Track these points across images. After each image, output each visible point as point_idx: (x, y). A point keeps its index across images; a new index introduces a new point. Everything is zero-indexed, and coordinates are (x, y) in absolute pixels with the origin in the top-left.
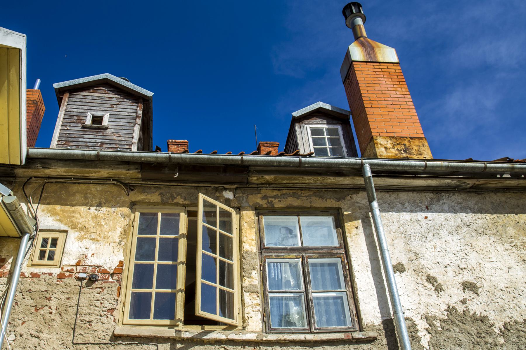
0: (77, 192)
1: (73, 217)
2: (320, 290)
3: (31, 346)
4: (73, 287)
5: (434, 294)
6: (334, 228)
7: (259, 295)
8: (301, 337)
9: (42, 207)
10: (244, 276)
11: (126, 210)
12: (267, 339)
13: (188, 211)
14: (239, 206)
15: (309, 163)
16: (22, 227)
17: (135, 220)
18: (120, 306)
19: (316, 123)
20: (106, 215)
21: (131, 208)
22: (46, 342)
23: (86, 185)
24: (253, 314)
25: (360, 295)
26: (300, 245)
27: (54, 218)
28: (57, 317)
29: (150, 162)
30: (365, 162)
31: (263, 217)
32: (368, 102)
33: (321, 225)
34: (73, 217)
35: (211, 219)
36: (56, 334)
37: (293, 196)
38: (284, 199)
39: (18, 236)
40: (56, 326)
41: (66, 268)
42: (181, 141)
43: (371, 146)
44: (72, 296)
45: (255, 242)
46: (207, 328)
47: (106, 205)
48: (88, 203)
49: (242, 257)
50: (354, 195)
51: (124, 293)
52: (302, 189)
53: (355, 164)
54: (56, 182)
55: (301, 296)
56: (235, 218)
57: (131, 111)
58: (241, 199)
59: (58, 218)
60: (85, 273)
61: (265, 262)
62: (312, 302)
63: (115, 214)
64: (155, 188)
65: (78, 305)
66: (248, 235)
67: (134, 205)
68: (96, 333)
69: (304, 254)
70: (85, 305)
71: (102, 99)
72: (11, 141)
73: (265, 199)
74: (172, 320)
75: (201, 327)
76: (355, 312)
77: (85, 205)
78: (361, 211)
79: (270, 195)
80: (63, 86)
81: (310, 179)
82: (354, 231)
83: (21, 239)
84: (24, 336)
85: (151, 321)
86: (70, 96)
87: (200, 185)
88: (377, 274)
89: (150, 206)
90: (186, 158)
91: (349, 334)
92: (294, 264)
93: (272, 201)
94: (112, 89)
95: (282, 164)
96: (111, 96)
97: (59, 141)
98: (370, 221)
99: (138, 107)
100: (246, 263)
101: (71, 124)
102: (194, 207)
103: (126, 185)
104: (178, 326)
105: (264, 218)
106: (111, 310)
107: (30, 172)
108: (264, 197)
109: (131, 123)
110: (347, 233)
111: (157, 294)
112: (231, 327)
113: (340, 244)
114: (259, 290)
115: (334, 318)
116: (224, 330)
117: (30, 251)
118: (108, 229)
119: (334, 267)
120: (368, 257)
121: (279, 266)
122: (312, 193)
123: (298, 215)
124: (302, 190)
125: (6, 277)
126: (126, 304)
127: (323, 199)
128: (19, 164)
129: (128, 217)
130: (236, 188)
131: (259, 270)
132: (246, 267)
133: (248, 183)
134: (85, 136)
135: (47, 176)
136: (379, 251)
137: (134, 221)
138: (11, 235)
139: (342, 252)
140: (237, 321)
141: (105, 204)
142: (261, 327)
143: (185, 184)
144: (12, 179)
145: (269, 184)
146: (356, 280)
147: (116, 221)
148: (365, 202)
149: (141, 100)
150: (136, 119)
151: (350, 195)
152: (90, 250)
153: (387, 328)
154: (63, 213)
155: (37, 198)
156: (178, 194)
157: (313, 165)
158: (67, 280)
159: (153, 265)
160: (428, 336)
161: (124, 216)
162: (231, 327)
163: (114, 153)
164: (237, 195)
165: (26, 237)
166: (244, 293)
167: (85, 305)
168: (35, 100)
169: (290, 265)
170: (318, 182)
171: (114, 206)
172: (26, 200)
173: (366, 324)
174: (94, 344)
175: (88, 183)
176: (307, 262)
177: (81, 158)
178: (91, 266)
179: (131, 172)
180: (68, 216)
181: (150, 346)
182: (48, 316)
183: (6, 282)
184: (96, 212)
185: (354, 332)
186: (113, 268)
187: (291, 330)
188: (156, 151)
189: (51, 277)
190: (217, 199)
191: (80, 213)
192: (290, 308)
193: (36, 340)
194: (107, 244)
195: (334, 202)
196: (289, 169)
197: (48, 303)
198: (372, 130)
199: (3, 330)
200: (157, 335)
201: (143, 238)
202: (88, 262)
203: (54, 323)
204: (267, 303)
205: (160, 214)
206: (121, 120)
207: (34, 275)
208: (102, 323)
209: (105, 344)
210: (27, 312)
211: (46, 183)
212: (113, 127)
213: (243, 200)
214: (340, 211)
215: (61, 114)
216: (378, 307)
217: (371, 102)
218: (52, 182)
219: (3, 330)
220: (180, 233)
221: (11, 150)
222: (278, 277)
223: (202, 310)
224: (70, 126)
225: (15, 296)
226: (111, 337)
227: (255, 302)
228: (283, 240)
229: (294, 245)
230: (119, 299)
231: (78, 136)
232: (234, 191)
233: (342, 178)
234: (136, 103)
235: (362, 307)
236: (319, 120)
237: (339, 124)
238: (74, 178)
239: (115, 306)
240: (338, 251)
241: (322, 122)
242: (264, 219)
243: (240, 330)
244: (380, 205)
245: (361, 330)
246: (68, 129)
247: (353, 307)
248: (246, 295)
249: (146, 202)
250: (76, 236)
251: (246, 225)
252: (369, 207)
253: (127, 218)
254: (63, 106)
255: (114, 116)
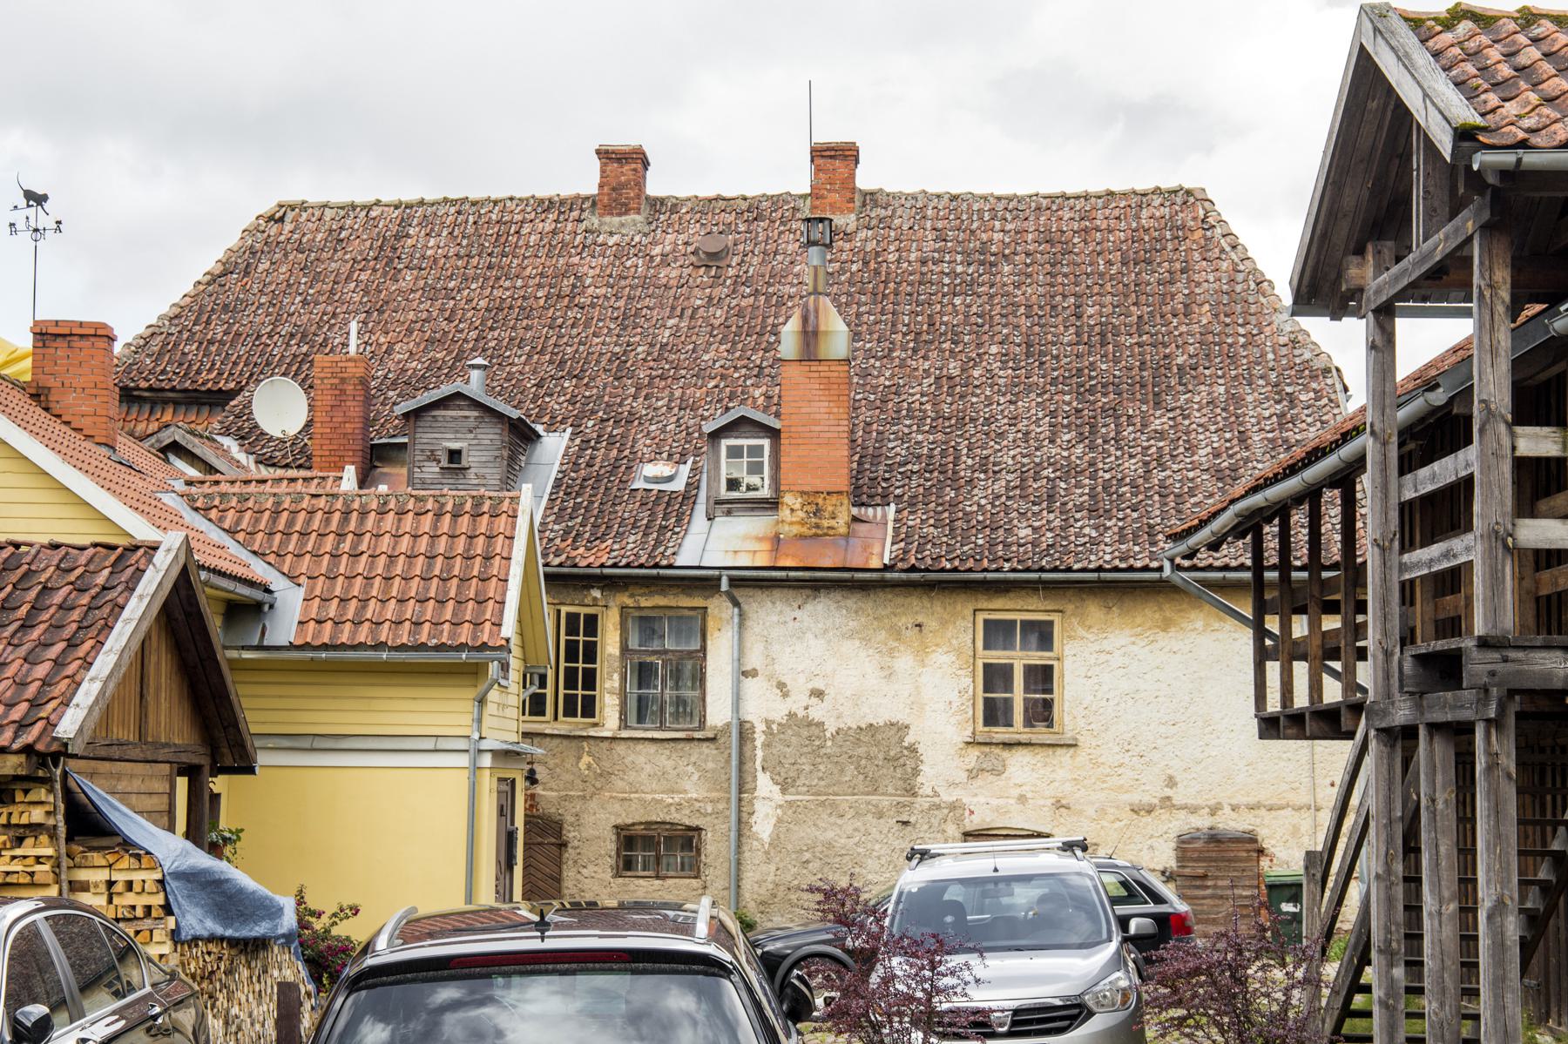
5: (779, 698)
160: (1172, 885)
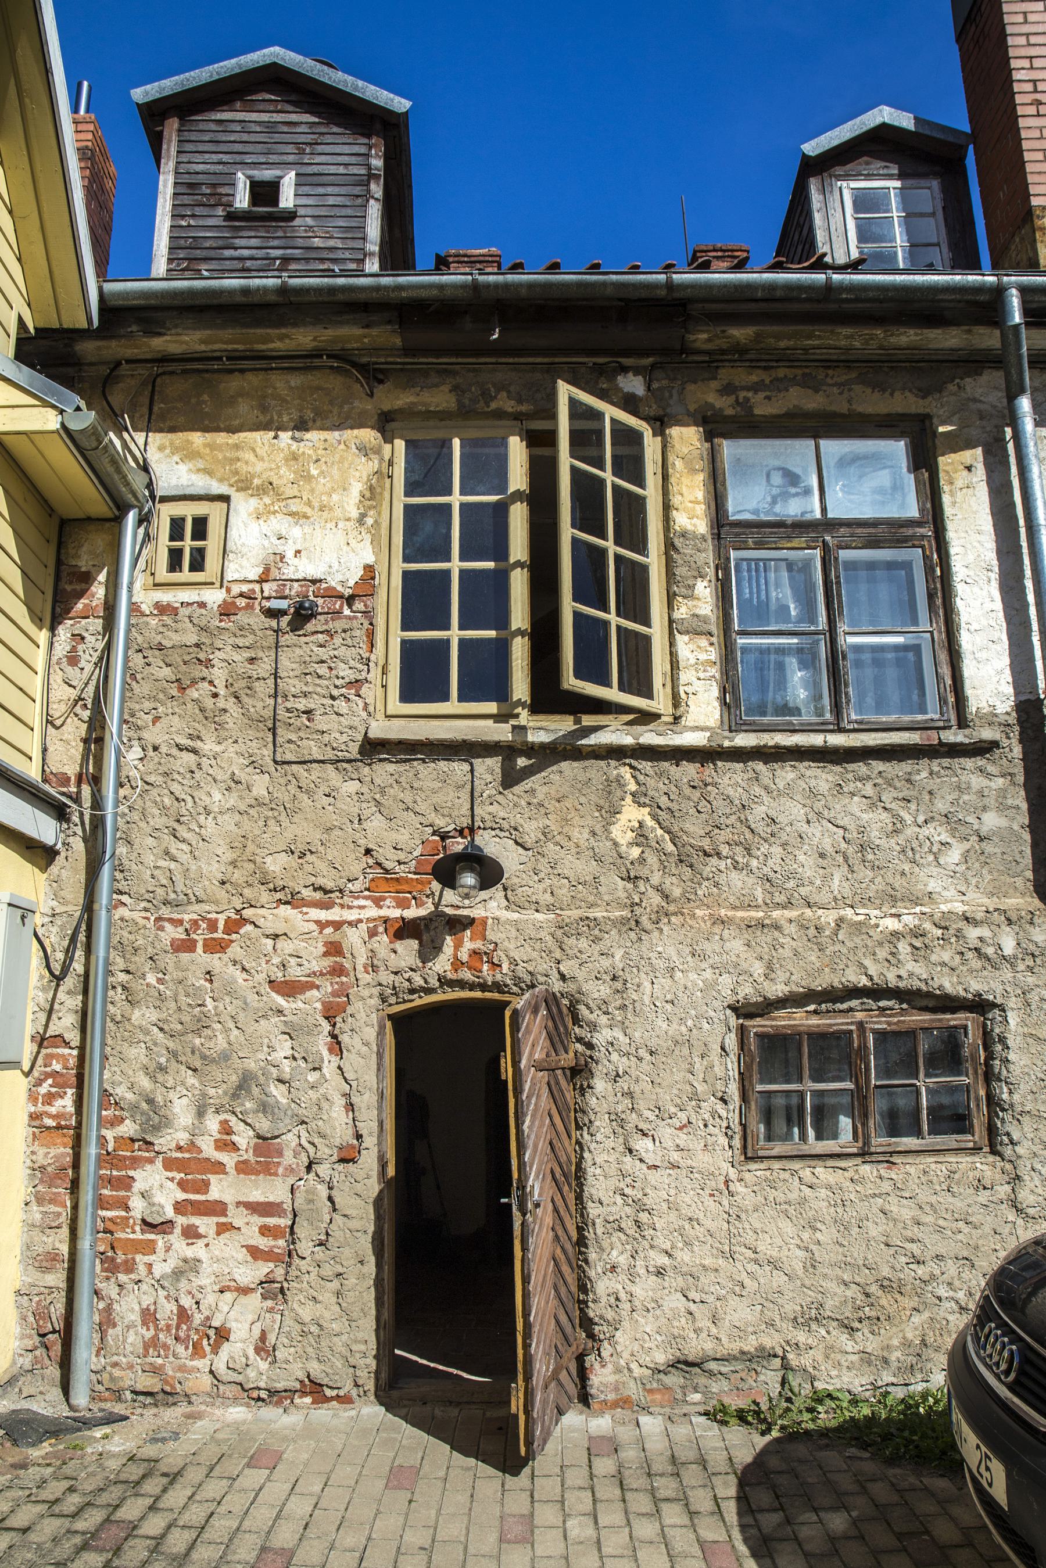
0: (241, 395)
1: (238, 460)
2: (864, 629)
3: (182, 770)
4: (259, 633)
6: (909, 471)
7: (714, 640)
8: (817, 740)
9: (156, 439)
10: (675, 594)
11: (369, 435)
12: (732, 744)
13: (527, 431)
14: (661, 413)
15: (852, 288)
16: (119, 491)
17: (395, 460)
18: (375, 674)
19: (868, 175)
20: (320, 452)
21: (382, 430)
22: (213, 762)
23: (261, 375)
24: (698, 686)
25: (966, 640)
26: (818, 515)
27: (191, 465)
28: (231, 704)
29: (423, 300)
30: (1009, 283)
31: (725, 443)
32: (1028, 98)
33: (874, 460)
34: (238, 460)
35: (592, 452)
36: (236, 742)
37: (804, 385)
38: (780, 391)
39: (110, 515)
40: (231, 725)
41: (236, 589)
42: (481, 251)
43: (1022, 239)
44: (260, 654)
45: (703, 507)
46: (588, 720)
47: (318, 423)
48: (271, 421)
49: (670, 546)
50: (968, 380)
51: (384, 642)
52: (828, 364)
53: (980, 289)
54: (185, 372)
55: (818, 641)
56: (651, 445)
57: (353, 160)
58: (667, 394)
59: (201, 464)
60: (285, 598)
61: (728, 559)
62: (844, 658)
63: (342, 446)
64: (438, 372)
65: (276, 676)
66: (684, 490)
67: (388, 421)
68: (326, 738)
69: (828, 538)
70: (291, 674)
71: (271, 127)
72: (54, 263)
73: (728, 395)
74: (503, 704)
75: (572, 718)
76: (949, 682)
77: (265, 427)
78: (984, 423)
79: (743, 383)
80: (158, 96)
81: (851, 337)
82: (962, 478)
83: (120, 523)
84: (164, 749)
85: (453, 707)
86: (181, 125)
87: (557, 360)
88: (1012, 589)
89: (431, 423)
90: (519, 285)
91: (933, 734)
92: (800, 565)
93: (747, 400)
94: (293, 98)
95: (779, 294)
96: (294, 117)
97: (170, 260)
98: (1006, 450)
99: (370, 149)
100: (680, 562)
101: (197, 209)
102: (543, 419)
103: (363, 368)
104: (517, 716)
105: (728, 446)
106: (356, 684)
107: (116, 349)
108: (728, 389)
109: (357, 196)
110: (942, 482)
111: (462, 642)
112: (646, 717)
113: (921, 510)
114: (714, 629)
115: (894, 696)
116: (629, 723)
117: (145, 552)
118: (329, 485)
119: (903, 572)
120: (992, 545)
121: (762, 569)
122: (854, 375)
123: (816, 436)
124: (829, 367)
125: (98, 617)
126: (390, 668)
127: (884, 390)
128: (86, 326)
129: (375, 453)
130: (653, 366)
131: (713, 579)
132: (680, 571)
133: (685, 349)
134: (238, 242)
135: (159, 356)
136: (1023, 531)
137: (391, 463)
138: (93, 515)
139: (928, 531)
140: (660, 703)
141: (314, 421)
142: (717, 715)
143: (516, 360)
144: (70, 371)
145: (739, 353)
146: (959, 604)
147: (346, 465)
148: (997, 398)
149: (378, 126)
150: (368, 185)
151: (957, 381)
152: (290, 542)
153: (1026, 721)
154: (212, 450)
155: (142, 416)
156: (501, 387)
157: (863, 295)
158: (242, 618)
159: (447, 573)
161: (364, 450)
162: (646, 717)
163: (326, 280)
164: (655, 385)
165: (131, 517)
166: (678, 636)
167: (291, 674)
168: (87, 147)
169: (790, 566)
170: (874, 344)
171: (338, 427)
172: (115, 424)
173: (974, 710)
174: (323, 762)
175: (266, 370)
176: (836, 559)
177: (240, 299)
178: (297, 581)
179: (374, 332)
180: (225, 458)
181: (455, 764)
182: (209, 703)
183: (100, 629)
184: (295, 446)
185: (944, 728)
186: (351, 583)
187: (791, 723)
188: (437, 268)
189: (203, 611)
190: (602, 395)
191: (254, 450)
192: (788, 672)
193: (189, 758)
194: (329, 525)
195: (912, 398)
196: (795, 307)
197: (205, 673)
198: (1032, 190)
199: (115, 737)
200: (471, 737)
201: (417, 505)
202: (289, 572)
203: (226, 717)
204: (734, 659)
205: (456, 443)
206: (330, 190)
207: (162, 609)
208: (337, 714)
209: (349, 761)
210: (161, 696)
211: (158, 375)
212: (310, 211)
213: (671, 396)
214: (927, 423)
215: (166, 181)
216: (1008, 671)
217: (1038, 96)
218: (172, 373)
219: (115, 737)
220: (512, 489)
221: (59, 290)
222: (758, 597)
223: (578, 675)
224: (193, 216)
225: (126, 659)
226: (362, 746)
227: (703, 657)
228: (774, 502)
229: (802, 514)
230: (373, 657)
231: (220, 243)
232: (648, 374)
233: (939, 331)
234: (363, 135)
235: (969, 669)
236: (877, 165)
237: (936, 175)
238: (228, 359)
239: (364, 674)
240: (918, 530)
241: (885, 171)
242: (728, 448)
243: (666, 723)
244: (1036, 406)
245: (963, 723)
246: (189, 226)
247: (946, 671)
248: (681, 640)
249: (420, 413)
250: (252, 509)
251: (679, 464)
252: (1006, 412)
253: (372, 456)
254: (169, 157)
255: (309, 178)
